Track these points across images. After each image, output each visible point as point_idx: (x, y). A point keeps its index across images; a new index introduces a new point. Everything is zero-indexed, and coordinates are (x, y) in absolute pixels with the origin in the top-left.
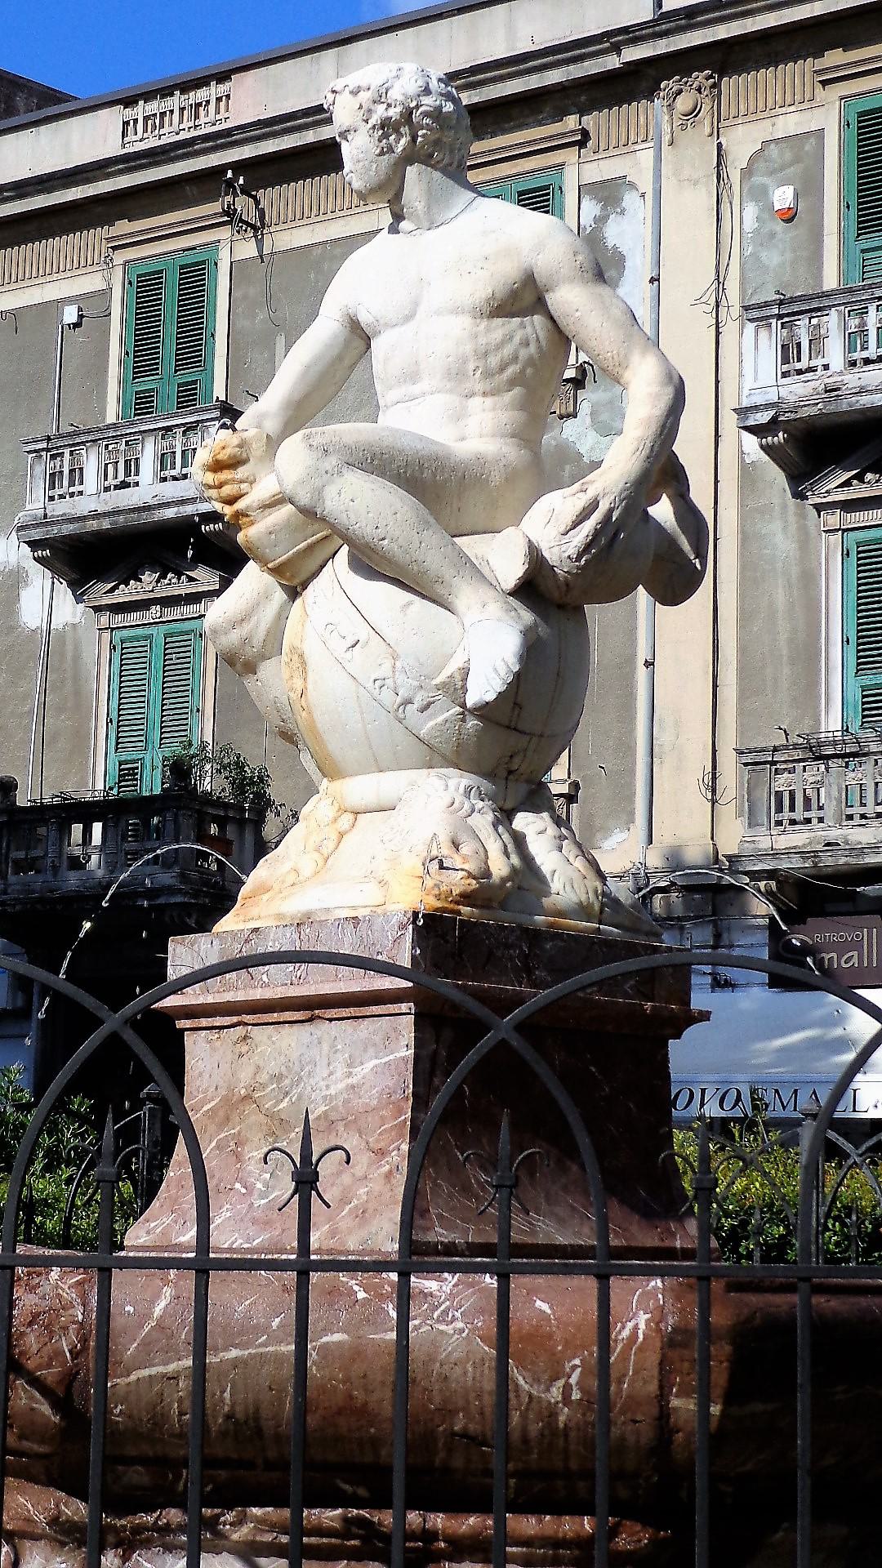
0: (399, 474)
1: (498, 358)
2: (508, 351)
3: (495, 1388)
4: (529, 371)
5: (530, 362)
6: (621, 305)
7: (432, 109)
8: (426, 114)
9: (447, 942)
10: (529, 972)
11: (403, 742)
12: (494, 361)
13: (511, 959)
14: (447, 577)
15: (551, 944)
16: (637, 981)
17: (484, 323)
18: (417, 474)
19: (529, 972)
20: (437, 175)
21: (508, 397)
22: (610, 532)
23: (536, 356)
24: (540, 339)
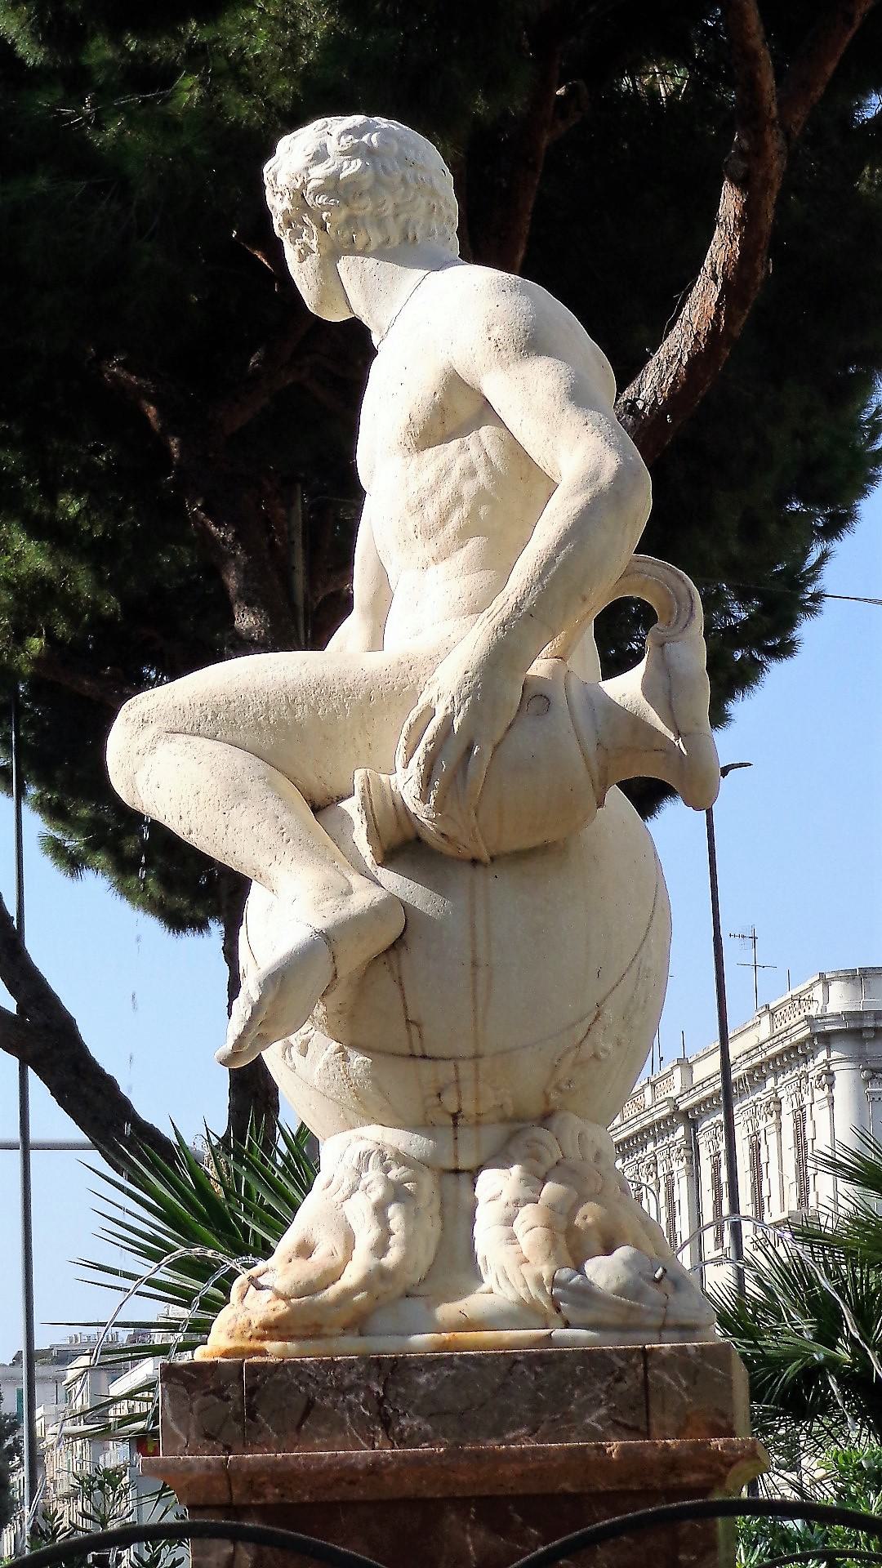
0: (259, 724)
1: (436, 506)
2: (446, 491)
4: (483, 511)
5: (481, 496)
7: (322, 182)
8: (318, 191)
12: (432, 511)
14: (263, 868)
16: (612, 1408)
17: (415, 460)
18: (287, 717)
19: (387, 1424)
20: (371, 262)
21: (461, 557)
22: (454, 750)
23: (488, 486)
24: (494, 460)
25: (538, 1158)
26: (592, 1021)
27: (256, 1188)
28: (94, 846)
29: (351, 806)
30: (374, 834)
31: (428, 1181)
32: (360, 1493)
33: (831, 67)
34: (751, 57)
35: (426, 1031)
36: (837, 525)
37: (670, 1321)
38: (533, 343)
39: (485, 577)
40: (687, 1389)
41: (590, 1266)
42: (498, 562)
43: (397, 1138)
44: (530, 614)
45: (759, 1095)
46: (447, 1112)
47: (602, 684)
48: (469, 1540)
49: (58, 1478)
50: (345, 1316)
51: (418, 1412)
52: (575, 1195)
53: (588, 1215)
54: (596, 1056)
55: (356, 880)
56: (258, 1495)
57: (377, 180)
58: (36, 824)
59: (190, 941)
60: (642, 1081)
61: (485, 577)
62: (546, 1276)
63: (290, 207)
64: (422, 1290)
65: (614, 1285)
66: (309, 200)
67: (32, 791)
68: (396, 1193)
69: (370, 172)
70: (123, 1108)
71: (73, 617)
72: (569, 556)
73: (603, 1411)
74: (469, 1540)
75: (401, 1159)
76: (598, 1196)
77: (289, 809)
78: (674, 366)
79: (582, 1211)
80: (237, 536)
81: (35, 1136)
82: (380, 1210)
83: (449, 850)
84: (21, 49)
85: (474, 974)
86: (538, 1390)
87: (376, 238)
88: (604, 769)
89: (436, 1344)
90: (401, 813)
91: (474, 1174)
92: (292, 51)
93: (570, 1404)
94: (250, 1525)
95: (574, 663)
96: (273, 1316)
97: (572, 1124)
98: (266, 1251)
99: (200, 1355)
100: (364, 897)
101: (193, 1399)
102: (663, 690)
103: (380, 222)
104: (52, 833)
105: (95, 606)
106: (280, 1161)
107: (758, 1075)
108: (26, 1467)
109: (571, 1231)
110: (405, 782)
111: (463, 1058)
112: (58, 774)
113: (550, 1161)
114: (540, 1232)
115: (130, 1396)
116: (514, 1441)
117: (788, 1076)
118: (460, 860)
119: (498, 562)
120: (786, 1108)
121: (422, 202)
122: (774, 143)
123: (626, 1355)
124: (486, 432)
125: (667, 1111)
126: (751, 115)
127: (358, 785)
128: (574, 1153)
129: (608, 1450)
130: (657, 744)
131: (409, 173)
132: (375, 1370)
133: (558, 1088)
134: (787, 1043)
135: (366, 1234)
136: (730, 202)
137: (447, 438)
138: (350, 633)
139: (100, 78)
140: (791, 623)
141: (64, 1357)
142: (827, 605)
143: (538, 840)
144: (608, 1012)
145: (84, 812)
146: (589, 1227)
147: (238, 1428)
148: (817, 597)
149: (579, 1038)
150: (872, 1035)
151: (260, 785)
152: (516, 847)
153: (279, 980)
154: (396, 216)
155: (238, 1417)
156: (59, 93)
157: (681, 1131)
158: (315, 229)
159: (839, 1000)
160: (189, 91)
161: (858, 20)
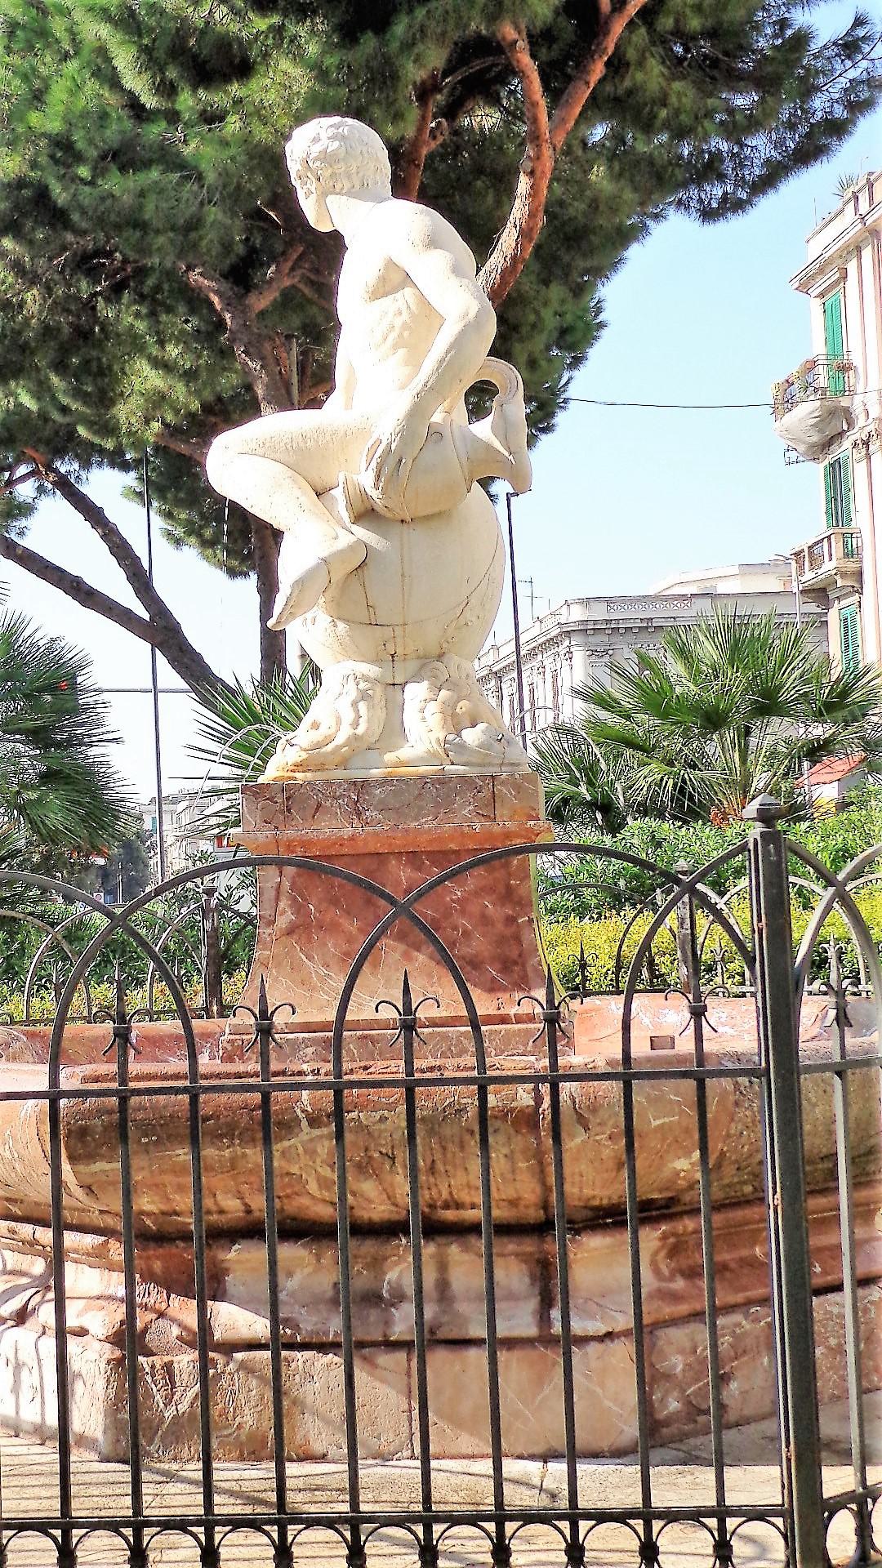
3: (638, 1434)
4: (406, 334)
5: (405, 326)
6: (333, 730)
11: (379, 102)
19: (359, 814)
22: (392, 461)
23: (408, 321)
27: (278, 707)
28: (189, 533)
29: (338, 493)
30: (350, 504)
31: (379, 690)
32: (345, 851)
33: (578, 110)
34: (535, 105)
35: (377, 611)
36: (577, 362)
37: (506, 761)
38: (432, 242)
39: (407, 370)
41: (465, 733)
42: (415, 362)
43: (366, 669)
45: (534, 664)
46: (388, 653)
47: (472, 427)
49: (174, 861)
50: (337, 760)
52: (456, 697)
53: (463, 706)
54: (466, 624)
55: (342, 533)
56: (293, 852)
58: (158, 522)
59: (240, 582)
60: (487, 646)
61: (407, 370)
62: (442, 739)
63: (300, 168)
65: (476, 743)
66: (311, 164)
67: (155, 504)
68: (364, 696)
69: (343, 148)
70: (205, 669)
71: (177, 412)
75: (366, 679)
76: (467, 697)
78: (493, 275)
79: (460, 704)
80: (262, 367)
81: (160, 686)
82: (355, 704)
83: (388, 515)
84: (143, 99)
87: (347, 186)
88: (471, 472)
90: (364, 494)
91: (403, 685)
92: (289, 102)
95: (454, 415)
96: (299, 760)
97: (454, 660)
98: (295, 728)
99: (261, 780)
100: (345, 540)
102: (504, 431)
103: (349, 177)
104: (166, 527)
105: (186, 406)
106: (291, 694)
107: (533, 653)
108: (159, 856)
109: (454, 715)
110: (367, 480)
112: (169, 496)
114: (438, 716)
115: (216, 814)
117: (549, 653)
118: (394, 521)
119: (415, 362)
120: (548, 671)
121: (372, 165)
122: (547, 152)
123: (483, 777)
124: (408, 291)
125: (486, 672)
126: (535, 137)
127: (341, 480)
128: (455, 674)
130: (499, 459)
131: (365, 149)
134: (548, 637)
135: (348, 716)
136: (523, 184)
137: (386, 295)
138: (334, 402)
139: (186, 116)
140: (552, 415)
141: (175, 801)
142: (572, 404)
143: (436, 510)
144: (473, 601)
145: (183, 516)
146: (463, 714)
147: (282, 817)
148: (566, 401)
150: (592, 632)
151: (288, 481)
152: (425, 514)
153: (301, 584)
154: (358, 173)
155: (282, 812)
156: (164, 124)
157: (493, 683)
158: (314, 180)
159: (577, 614)
160: (233, 125)
161: (592, 85)
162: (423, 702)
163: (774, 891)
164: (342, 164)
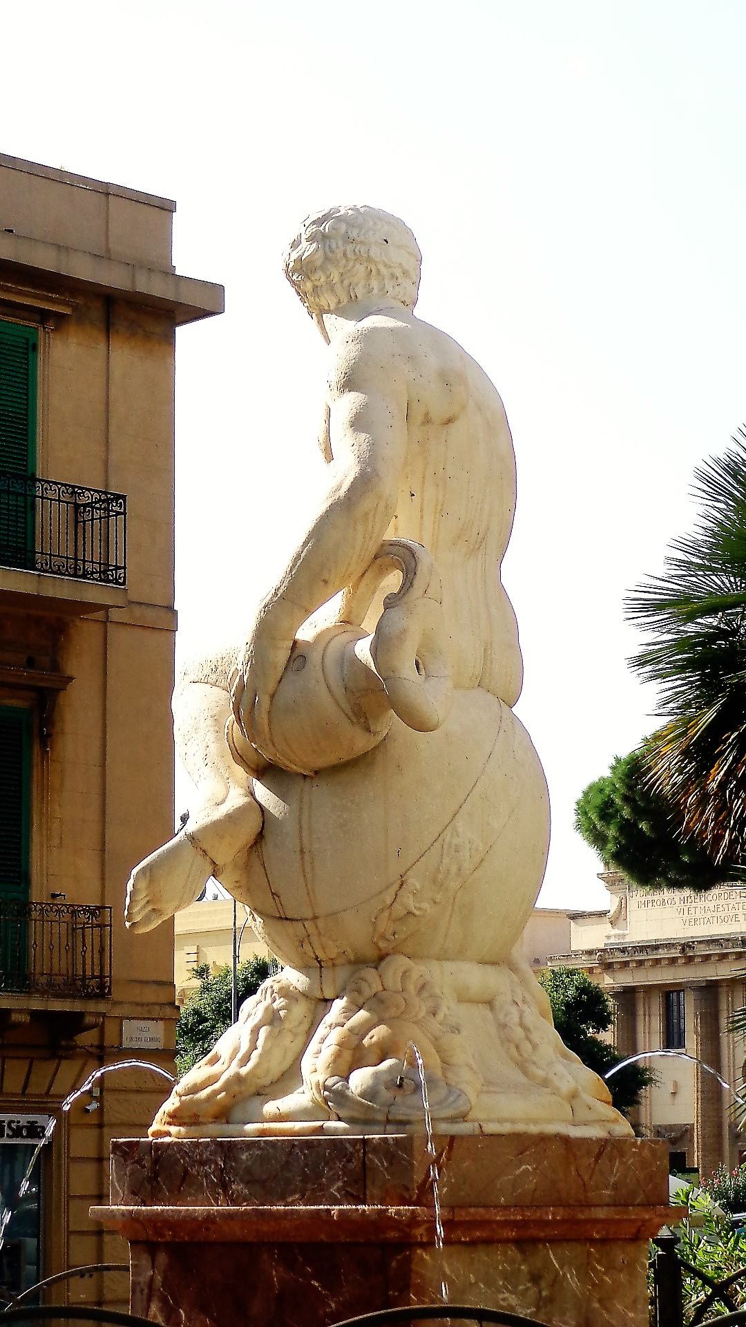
9: (144, 1167)
10: (225, 1186)
13: (207, 1176)
15: (247, 1154)
16: (344, 1182)
19: (225, 1186)
25: (359, 991)
26: (397, 888)
40: (387, 1169)
44: (282, 598)
48: (274, 1273)
50: (212, 1110)
51: (242, 1181)
52: (376, 1019)
57: (326, 258)
64: (267, 1090)
69: (321, 253)
72: (309, 552)
73: (340, 1184)
74: (274, 1273)
77: (218, 740)
85: (302, 859)
86: (305, 1167)
89: (259, 1130)
93: (322, 1178)
94: (478, 1234)
101: (127, 1166)
103: (332, 288)
109: (359, 1047)
111: (307, 920)
113: (368, 992)
116: (292, 1204)
121: (361, 269)
129: (332, 1212)
132: (220, 1150)
133: (383, 937)
146: (371, 1046)
149: (389, 902)
154: (342, 282)
162: (328, 1028)
163: (186, 1238)
164: (319, 274)
